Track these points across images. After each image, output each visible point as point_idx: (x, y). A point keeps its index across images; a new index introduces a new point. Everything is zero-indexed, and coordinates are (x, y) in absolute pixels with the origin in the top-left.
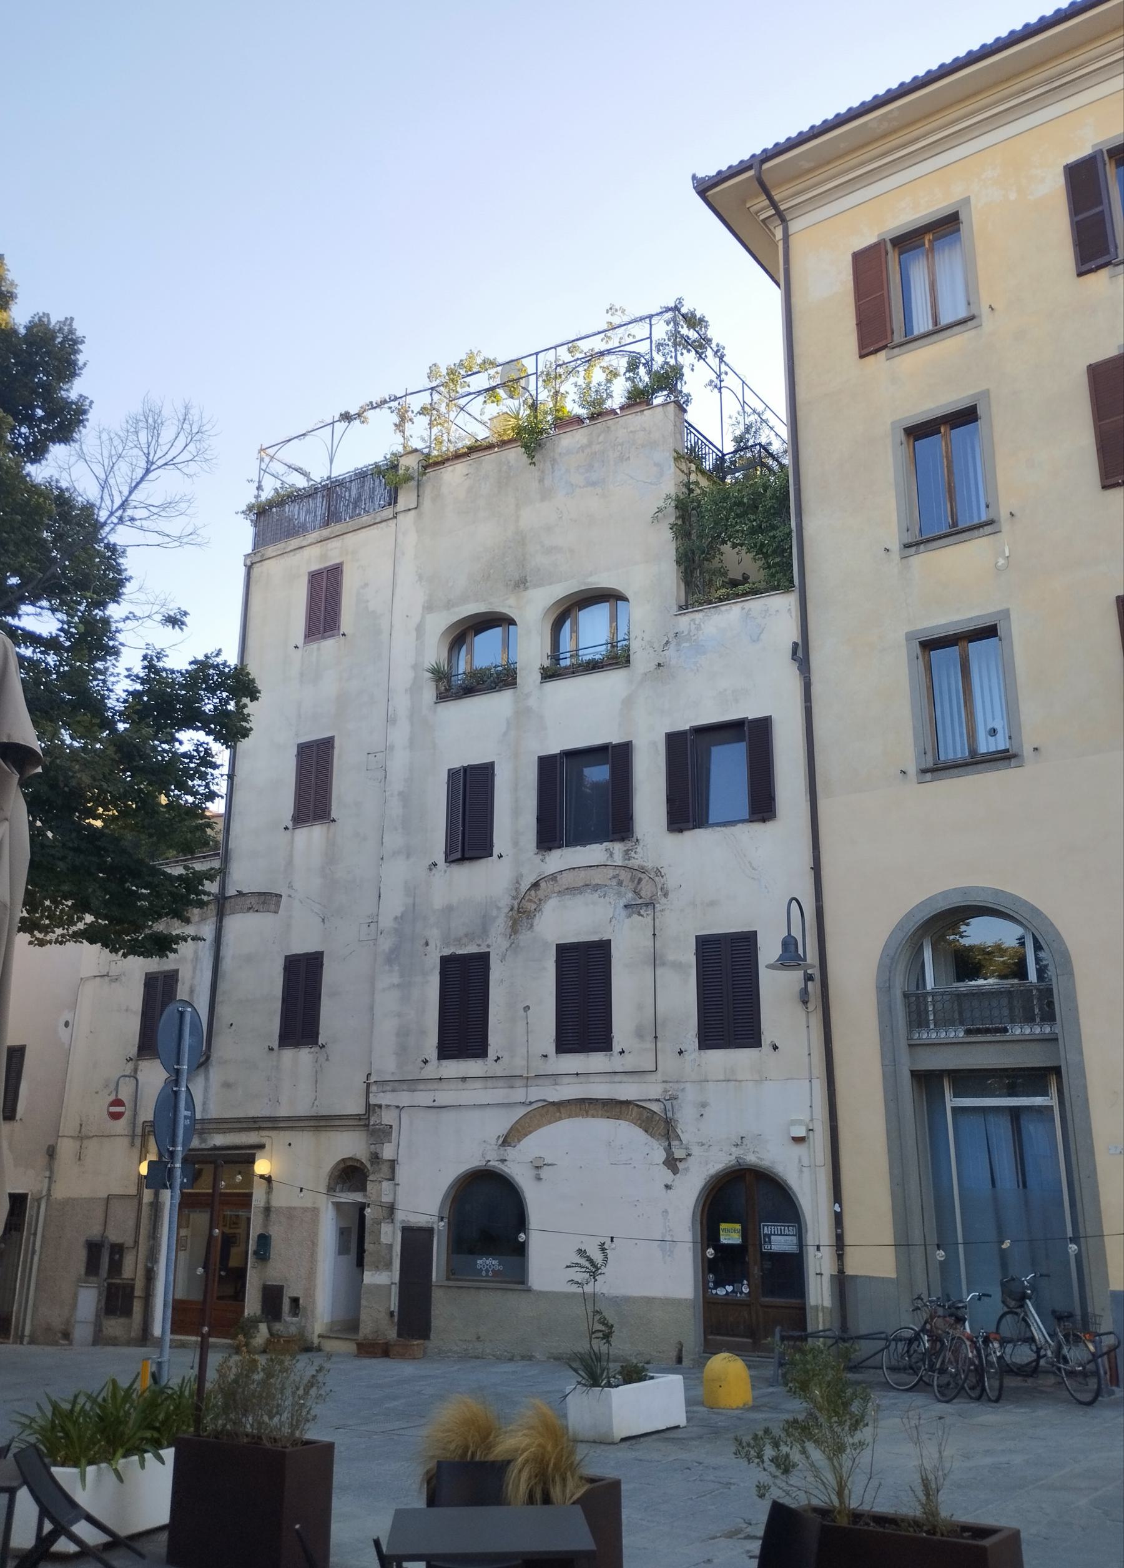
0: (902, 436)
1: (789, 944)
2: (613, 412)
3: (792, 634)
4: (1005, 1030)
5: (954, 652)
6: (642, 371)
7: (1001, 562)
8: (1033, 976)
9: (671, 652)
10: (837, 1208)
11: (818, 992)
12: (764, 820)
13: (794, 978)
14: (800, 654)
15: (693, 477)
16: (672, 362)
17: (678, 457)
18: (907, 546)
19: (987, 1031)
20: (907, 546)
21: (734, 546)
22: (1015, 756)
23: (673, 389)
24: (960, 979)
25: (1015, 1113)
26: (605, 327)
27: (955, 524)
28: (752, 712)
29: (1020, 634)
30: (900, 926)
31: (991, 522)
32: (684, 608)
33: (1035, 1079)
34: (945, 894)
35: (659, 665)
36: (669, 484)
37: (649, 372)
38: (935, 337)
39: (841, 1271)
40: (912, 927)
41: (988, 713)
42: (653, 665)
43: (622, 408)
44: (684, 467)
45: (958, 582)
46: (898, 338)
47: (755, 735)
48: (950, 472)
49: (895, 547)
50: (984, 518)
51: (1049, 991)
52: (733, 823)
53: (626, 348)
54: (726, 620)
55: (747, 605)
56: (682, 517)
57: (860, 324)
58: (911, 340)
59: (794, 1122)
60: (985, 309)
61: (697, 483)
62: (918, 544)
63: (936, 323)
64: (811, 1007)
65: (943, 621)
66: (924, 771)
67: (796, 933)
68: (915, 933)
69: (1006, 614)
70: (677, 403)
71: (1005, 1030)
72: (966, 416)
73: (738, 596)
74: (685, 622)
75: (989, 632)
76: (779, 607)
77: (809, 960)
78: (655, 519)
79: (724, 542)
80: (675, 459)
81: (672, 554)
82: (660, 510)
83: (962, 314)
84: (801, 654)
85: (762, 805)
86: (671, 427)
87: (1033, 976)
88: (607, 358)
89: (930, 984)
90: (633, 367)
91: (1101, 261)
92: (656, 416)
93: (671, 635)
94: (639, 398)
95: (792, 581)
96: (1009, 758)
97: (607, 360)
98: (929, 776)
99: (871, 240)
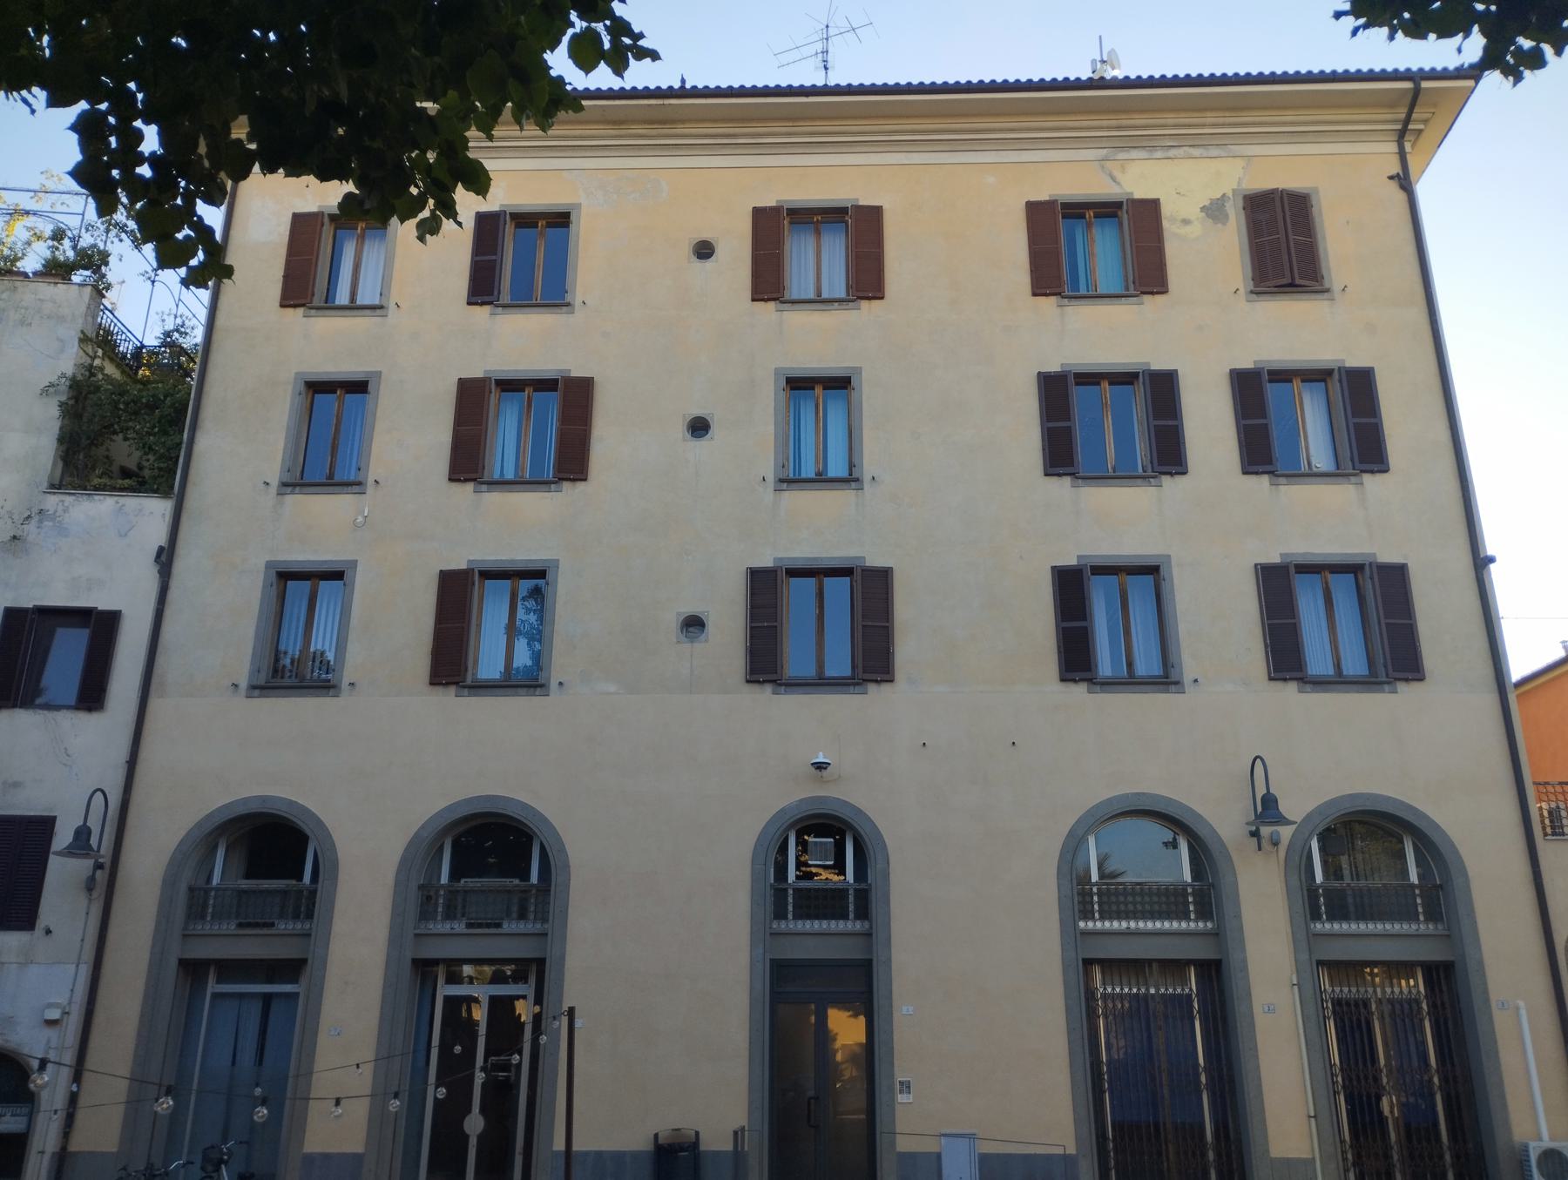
0: (302, 387)
1: (82, 834)
2: (25, 275)
3: (160, 537)
4: (272, 925)
5: (307, 585)
6: (67, 243)
7: (360, 519)
8: (534, 879)
9: (32, 527)
10: (74, 1088)
11: (105, 883)
12: (90, 710)
13: (83, 866)
14: (163, 558)
15: (97, 362)
16: (102, 246)
17: (84, 339)
18: (285, 485)
19: (257, 925)
20: (285, 485)
21: (126, 439)
22: (334, 687)
23: (97, 270)
24: (248, 876)
25: (268, 999)
26: (37, 187)
27: (331, 476)
28: (103, 602)
29: (362, 581)
30: (199, 825)
31: (359, 484)
32: (56, 486)
33: (292, 969)
34: (246, 801)
35: (15, 537)
36: (68, 361)
37: (74, 248)
38: (348, 312)
39: (64, 1148)
40: (218, 820)
41: (322, 641)
42: (7, 537)
43: (35, 274)
44: (90, 350)
45: (320, 527)
46: (317, 301)
47: (101, 628)
48: (337, 430)
49: (275, 483)
50: (352, 478)
51: (313, 893)
52: (58, 708)
53: (56, 216)
54: (96, 510)
55: (122, 500)
56: (76, 399)
57: (286, 277)
58: (328, 305)
59: (50, 1006)
60: (392, 305)
61: (102, 369)
62: (294, 485)
63: (353, 299)
64: (95, 894)
65: (301, 558)
66: (254, 687)
67: (94, 824)
68: (210, 833)
69: (354, 564)
70: (95, 287)
71: (272, 925)
72: (359, 387)
73: (114, 489)
74: (52, 502)
75: (338, 575)
76: (152, 512)
77: (102, 852)
78: (46, 391)
79: (115, 433)
80: (81, 341)
81: (56, 431)
82: (51, 385)
83: (377, 302)
84: (165, 559)
85: (92, 696)
86: (83, 308)
87: (534, 879)
88: (32, 218)
89: (216, 880)
90: (58, 235)
91: (487, 299)
92: (71, 294)
93: (35, 510)
94: (57, 270)
95: (172, 487)
96: (329, 688)
97: (30, 221)
98: (257, 692)
99: (313, 208)
